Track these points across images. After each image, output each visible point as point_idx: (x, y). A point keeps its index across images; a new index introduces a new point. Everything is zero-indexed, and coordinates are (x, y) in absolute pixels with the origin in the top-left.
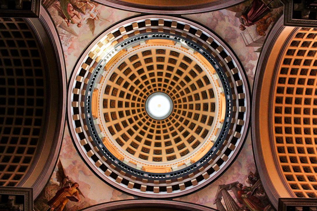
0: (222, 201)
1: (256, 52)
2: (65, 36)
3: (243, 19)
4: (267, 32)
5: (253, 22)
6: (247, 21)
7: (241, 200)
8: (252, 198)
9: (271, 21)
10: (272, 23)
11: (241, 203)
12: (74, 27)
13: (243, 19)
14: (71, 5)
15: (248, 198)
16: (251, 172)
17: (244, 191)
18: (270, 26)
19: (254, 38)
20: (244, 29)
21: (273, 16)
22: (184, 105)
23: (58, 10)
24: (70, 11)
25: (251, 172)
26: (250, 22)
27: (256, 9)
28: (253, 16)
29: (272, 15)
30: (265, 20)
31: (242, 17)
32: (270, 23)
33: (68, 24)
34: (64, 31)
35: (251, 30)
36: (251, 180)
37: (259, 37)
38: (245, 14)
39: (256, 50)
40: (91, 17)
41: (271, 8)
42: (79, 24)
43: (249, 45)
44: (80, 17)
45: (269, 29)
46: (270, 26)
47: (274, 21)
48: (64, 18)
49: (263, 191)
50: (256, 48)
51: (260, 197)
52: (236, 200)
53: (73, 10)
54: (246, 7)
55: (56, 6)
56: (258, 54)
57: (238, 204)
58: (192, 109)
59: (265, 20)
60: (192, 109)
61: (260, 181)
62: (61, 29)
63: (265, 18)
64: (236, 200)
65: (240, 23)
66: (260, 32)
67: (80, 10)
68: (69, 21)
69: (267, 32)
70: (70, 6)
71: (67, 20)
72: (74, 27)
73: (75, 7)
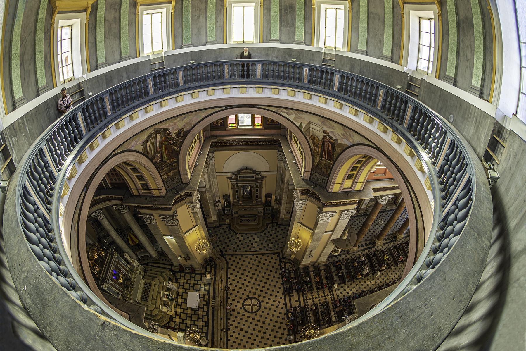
0: (148, 143)
1: (301, 124)
3: (331, 139)
7: (162, 143)
8: (168, 147)
11: (160, 148)
13: (331, 139)
15: (166, 146)
16: (184, 129)
17: (168, 138)
18: (312, 146)
20: (324, 132)
25: (184, 129)
26: (325, 140)
27: (329, 151)
28: (327, 146)
29: (318, 154)
35: (321, 136)
36: (178, 135)
37: (311, 134)
38: (333, 144)
39: (302, 124)
43: (310, 123)
45: (311, 144)
46: (312, 146)
49: (180, 147)
50: (304, 125)
51: (174, 149)
52: (158, 144)
56: (298, 124)
57: (158, 148)
59: (318, 148)
61: (184, 139)
63: (320, 149)
64: (158, 144)
65: (330, 135)
66: (314, 137)
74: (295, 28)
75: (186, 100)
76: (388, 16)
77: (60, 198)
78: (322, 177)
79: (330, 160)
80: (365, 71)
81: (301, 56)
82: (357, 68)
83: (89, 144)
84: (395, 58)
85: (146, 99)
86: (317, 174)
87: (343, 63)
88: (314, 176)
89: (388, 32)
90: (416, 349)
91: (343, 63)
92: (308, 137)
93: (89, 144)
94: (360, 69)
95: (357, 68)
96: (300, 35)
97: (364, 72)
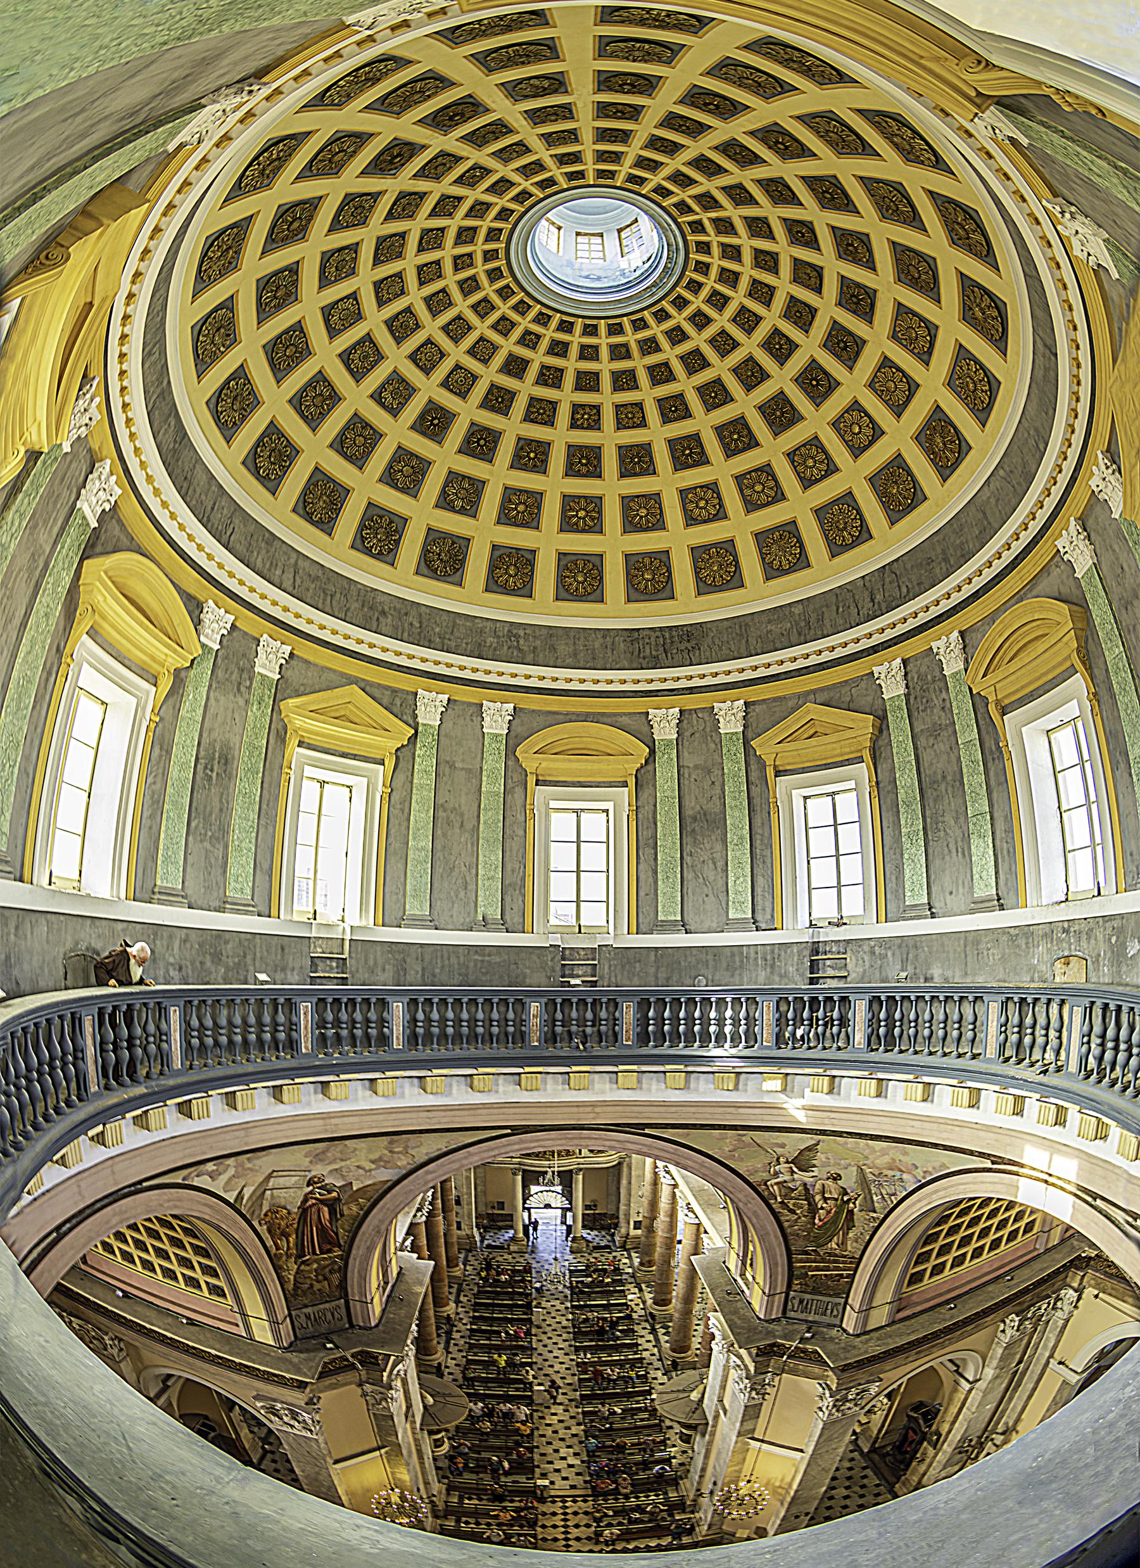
2: (884, 1192)
4: (263, 1230)
5: (304, 1210)
6: (316, 1199)
9: (277, 1249)
10: (273, 1250)
12: (849, 1181)
14: (817, 1221)
18: (269, 1243)
19: (272, 1195)
21: (284, 1258)
22: (631, 374)
23: (845, 1235)
24: (829, 1212)
27: (322, 1230)
28: (315, 1217)
29: (288, 1256)
30: (287, 1236)
31: (334, 1194)
32: (275, 1244)
33: (856, 1199)
34: (875, 1198)
40: (795, 1169)
41: (303, 1262)
42: (835, 1179)
44: (818, 1186)
46: (269, 1243)
47: (275, 1255)
48: (851, 1212)
53: (822, 1208)
54: (342, 1215)
55: (842, 1244)
56: (231, 1197)
58: (582, 357)
59: (287, 1236)
60: (582, 357)
62: (876, 1205)
67: (808, 1195)
68: (849, 1200)
69: (263, 1230)
70: (820, 1220)
71: (851, 1205)
72: (849, 1181)
73: (813, 1209)
74: (226, 847)
75: (402, 1096)
76: (491, 816)
77: (175, 1031)
78: (327, 1306)
79: (329, 1251)
80: (437, 971)
81: (249, 958)
82: (415, 970)
83: (139, 1112)
84: (512, 918)
85: (518, 1052)
86: (309, 1310)
87: (371, 963)
88: (303, 1319)
89: (490, 858)
90: (6, 1341)
91: (371, 963)
92: (255, 1223)
93: (139, 1112)
94: (423, 969)
95: (415, 970)
96: (240, 881)
97: (434, 976)
